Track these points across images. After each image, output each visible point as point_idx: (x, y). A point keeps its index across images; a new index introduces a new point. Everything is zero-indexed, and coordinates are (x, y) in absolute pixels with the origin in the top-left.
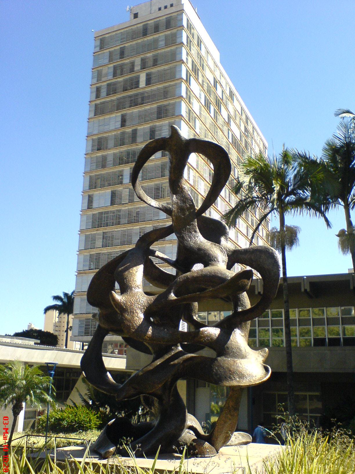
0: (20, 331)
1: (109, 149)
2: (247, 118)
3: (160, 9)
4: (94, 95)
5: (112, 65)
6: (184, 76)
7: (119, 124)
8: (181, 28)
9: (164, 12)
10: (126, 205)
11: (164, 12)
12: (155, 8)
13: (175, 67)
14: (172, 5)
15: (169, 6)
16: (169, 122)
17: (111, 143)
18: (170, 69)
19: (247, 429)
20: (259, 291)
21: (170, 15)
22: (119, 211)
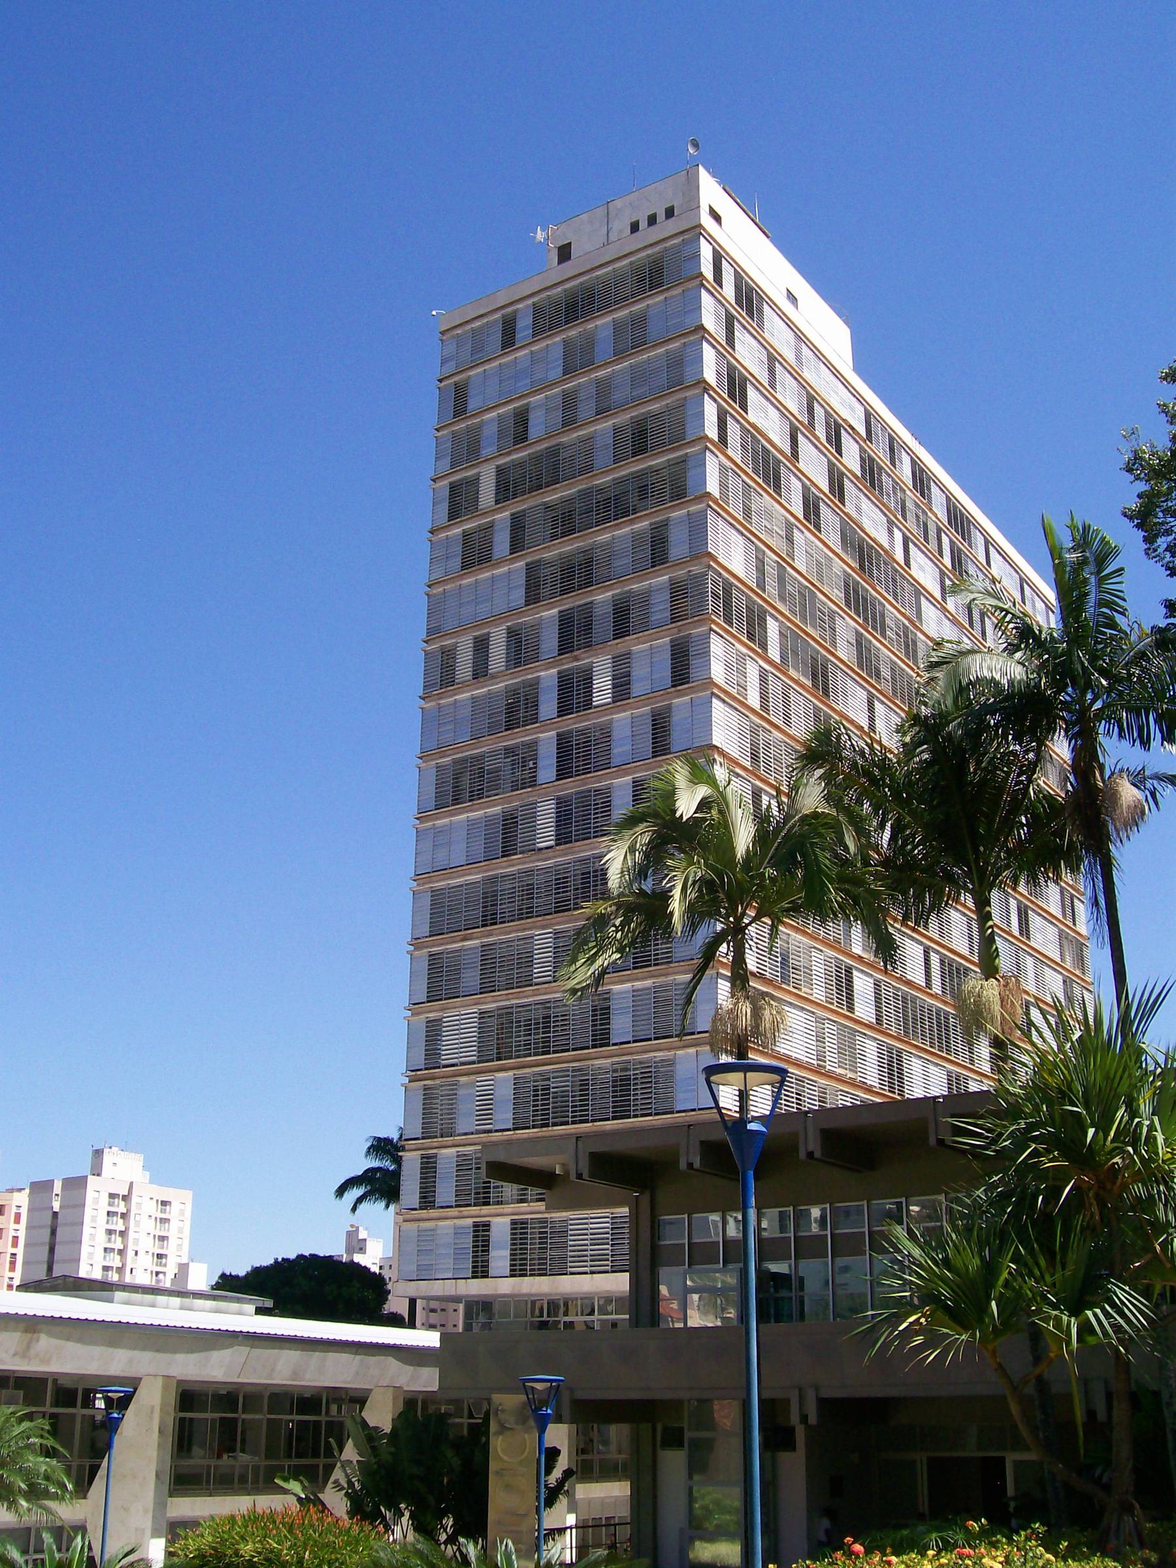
0: (241, 1270)
1: (493, 677)
2: (959, 520)
3: (635, 227)
4: (444, 508)
5: (457, 531)
6: (712, 432)
7: (519, 595)
8: (697, 282)
9: (649, 235)
10: (550, 853)
11: (649, 235)
12: (621, 226)
13: (682, 404)
14: (670, 213)
15: (661, 216)
16: (670, 579)
17: (603, 457)
18: (669, 410)
19: (650, 1425)
20: (810, 1148)
21: (657, 249)
22: (529, 872)
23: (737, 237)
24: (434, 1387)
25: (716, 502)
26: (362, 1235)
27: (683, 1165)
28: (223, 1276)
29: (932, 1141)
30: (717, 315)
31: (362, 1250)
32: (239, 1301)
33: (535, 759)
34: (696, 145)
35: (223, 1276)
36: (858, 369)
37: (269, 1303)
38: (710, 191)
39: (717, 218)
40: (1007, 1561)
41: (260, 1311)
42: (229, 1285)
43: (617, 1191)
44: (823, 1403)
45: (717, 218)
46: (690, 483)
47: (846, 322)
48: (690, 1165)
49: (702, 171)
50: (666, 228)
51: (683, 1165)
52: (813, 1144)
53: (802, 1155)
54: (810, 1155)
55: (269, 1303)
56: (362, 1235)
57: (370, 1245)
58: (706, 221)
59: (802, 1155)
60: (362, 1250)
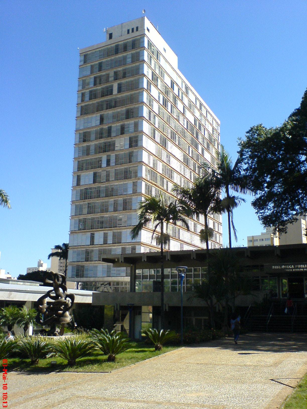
0: (24, 273)
4: (80, 99)
6: (145, 86)
9: (132, 35)
22: (99, 187)
23: (153, 35)
24: (91, 302)
25: (145, 104)
26: (42, 262)
27: (143, 260)
28: (20, 275)
29: (192, 258)
30: (148, 57)
31: (42, 266)
32: (36, 283)
33: (101, 161)
34: (145, 11)
35: (20, 275)
36: (179, 68)
37: (42, 284)
38: (147, 24)
39: (148, 30)
40: (306, 279)
41: (40, 285)
42: (21, 278)
43: (128, 265)
44: (169, 307)
45: (148, 30)
46: (140, 99)
47: (177, 55)
48: (144, 261)
49: (146, 18)
50: (136, 34)
51: (143, 260)
52: (169, 257)
53: (167, 259)
54: (168, 260)
55: (42, 284)
56: (42, 262)
57: (43, 265)
58: (146, 32)
59: (167, 259)
60: (42, 266)
